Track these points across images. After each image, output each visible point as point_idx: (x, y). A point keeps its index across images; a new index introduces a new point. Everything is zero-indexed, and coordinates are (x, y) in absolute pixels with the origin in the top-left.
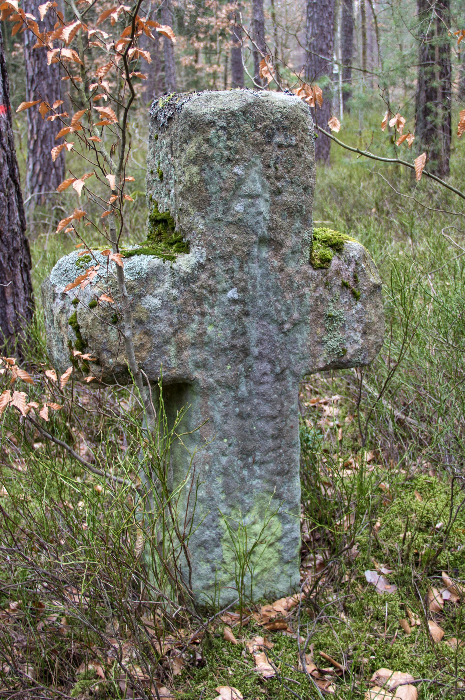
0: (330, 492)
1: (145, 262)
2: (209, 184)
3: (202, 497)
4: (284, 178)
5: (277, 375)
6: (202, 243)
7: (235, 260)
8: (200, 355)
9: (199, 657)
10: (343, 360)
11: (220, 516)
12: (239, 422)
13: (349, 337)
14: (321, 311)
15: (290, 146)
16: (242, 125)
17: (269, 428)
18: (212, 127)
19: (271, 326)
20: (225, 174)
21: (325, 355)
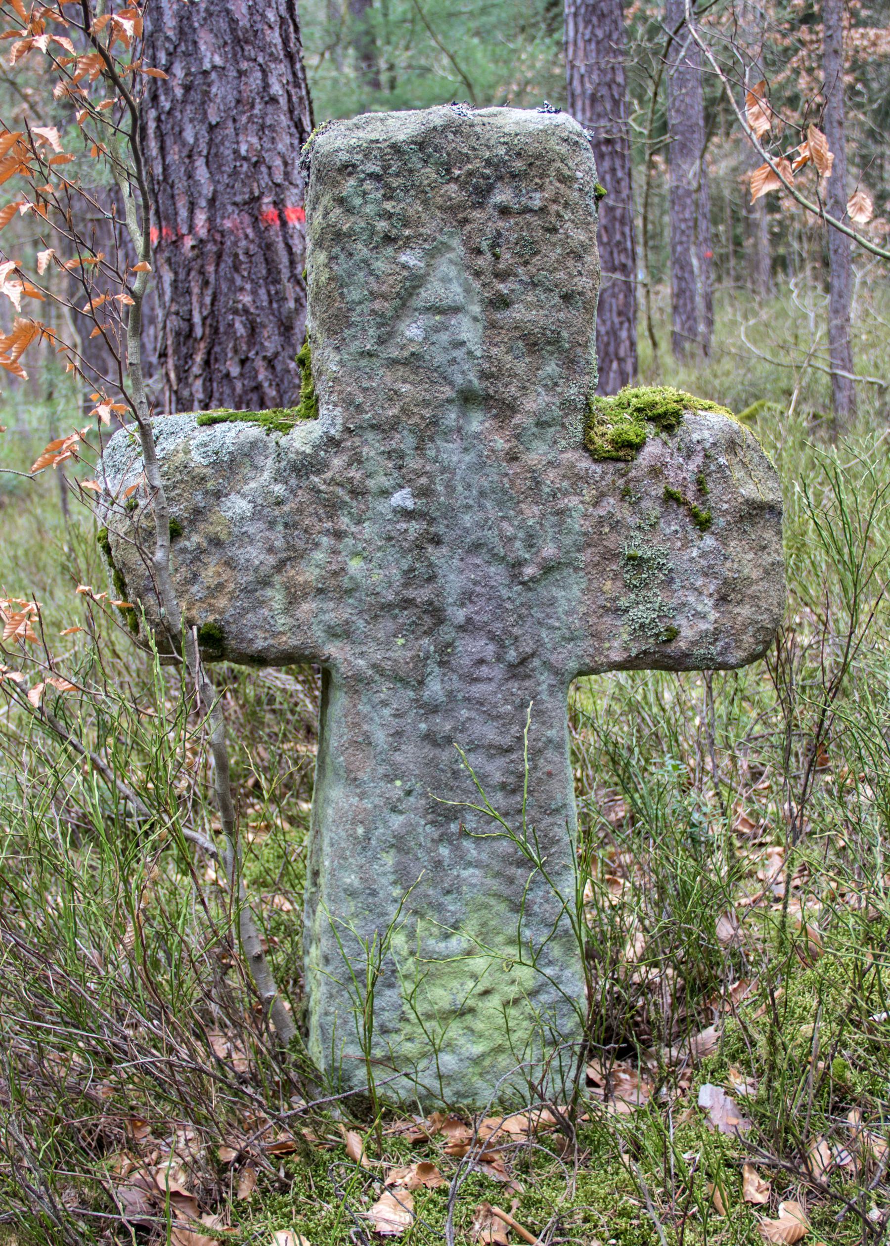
2: (348, 285)
3: (351, 885)
4: (516, 275)
5: (511, 666)
6: (334, 397)
7: (405, 433)
8: (335, 613)
10: (671, 649)
12: (428, 751)
13: (684, 605)
14: (612, 547)
15: (527, 210)
16: (419, 171)
17: (496, 771)
18: (350, 174)
19: (493, 569)
20: (380, 265)
21: (625, 637)
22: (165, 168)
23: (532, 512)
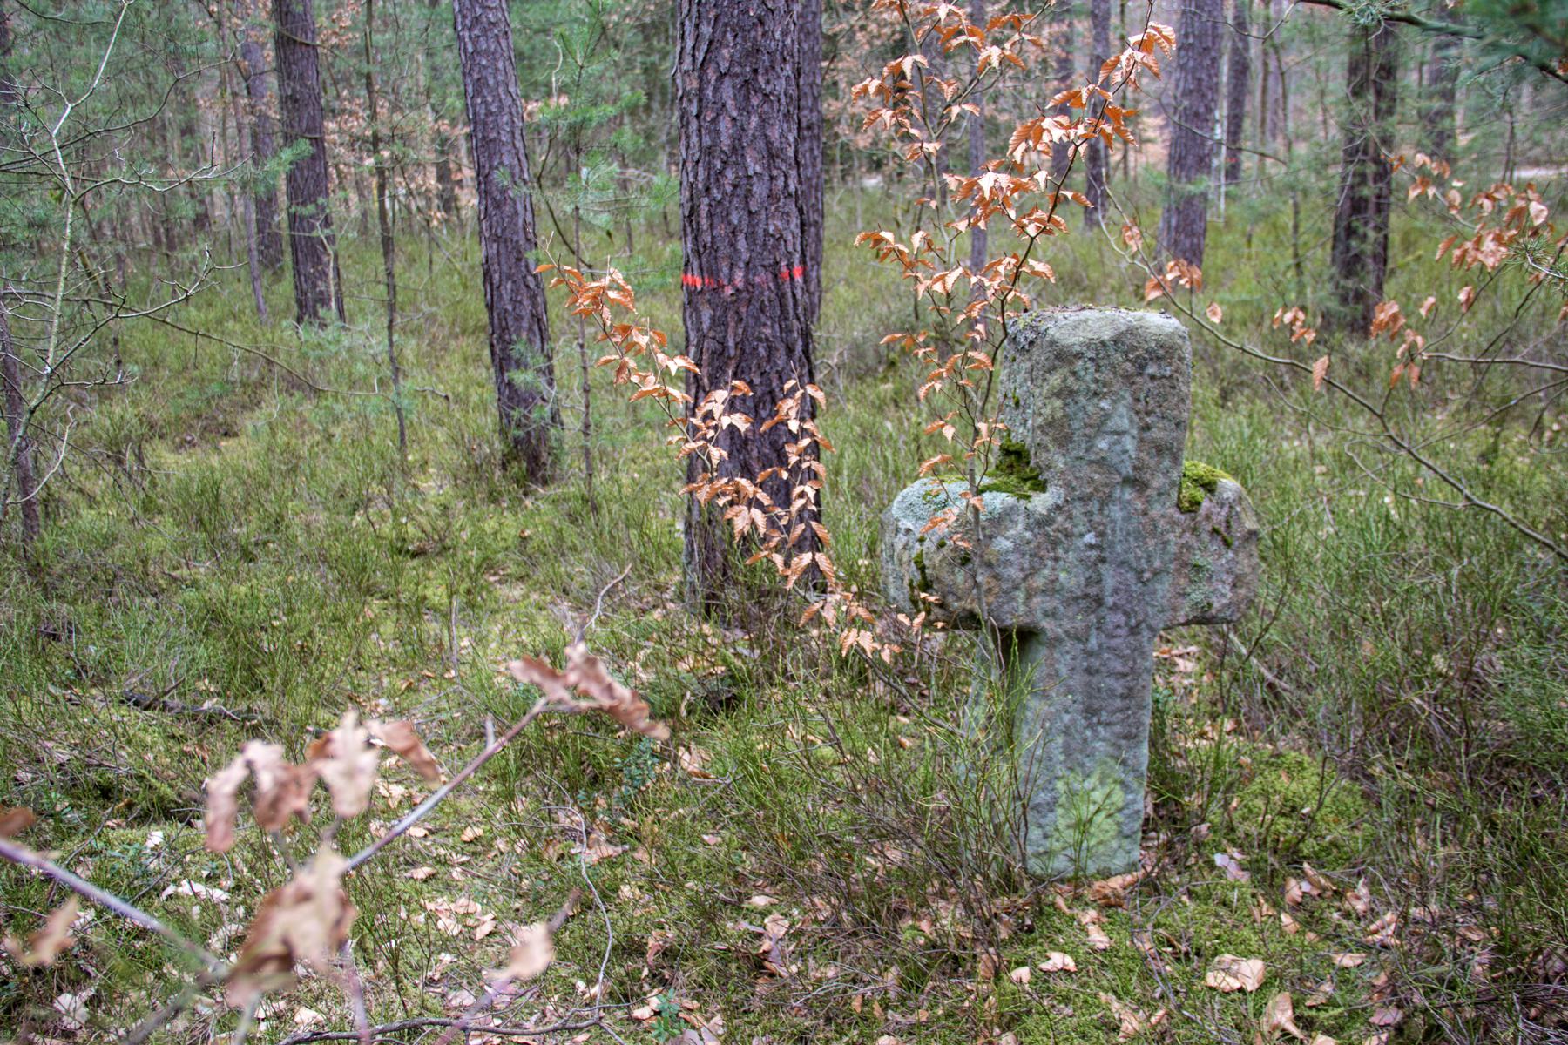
0: (1180, 763)
1: (997, 501)
8: (1050, 603)
9: (1028, 922)
10: (1208, 615)
11: (1057, 778)
12: (1086, 678)
15: (1164, 377)
20: (1090, 409)
22: (713, 238)
23: (1151, 542)
